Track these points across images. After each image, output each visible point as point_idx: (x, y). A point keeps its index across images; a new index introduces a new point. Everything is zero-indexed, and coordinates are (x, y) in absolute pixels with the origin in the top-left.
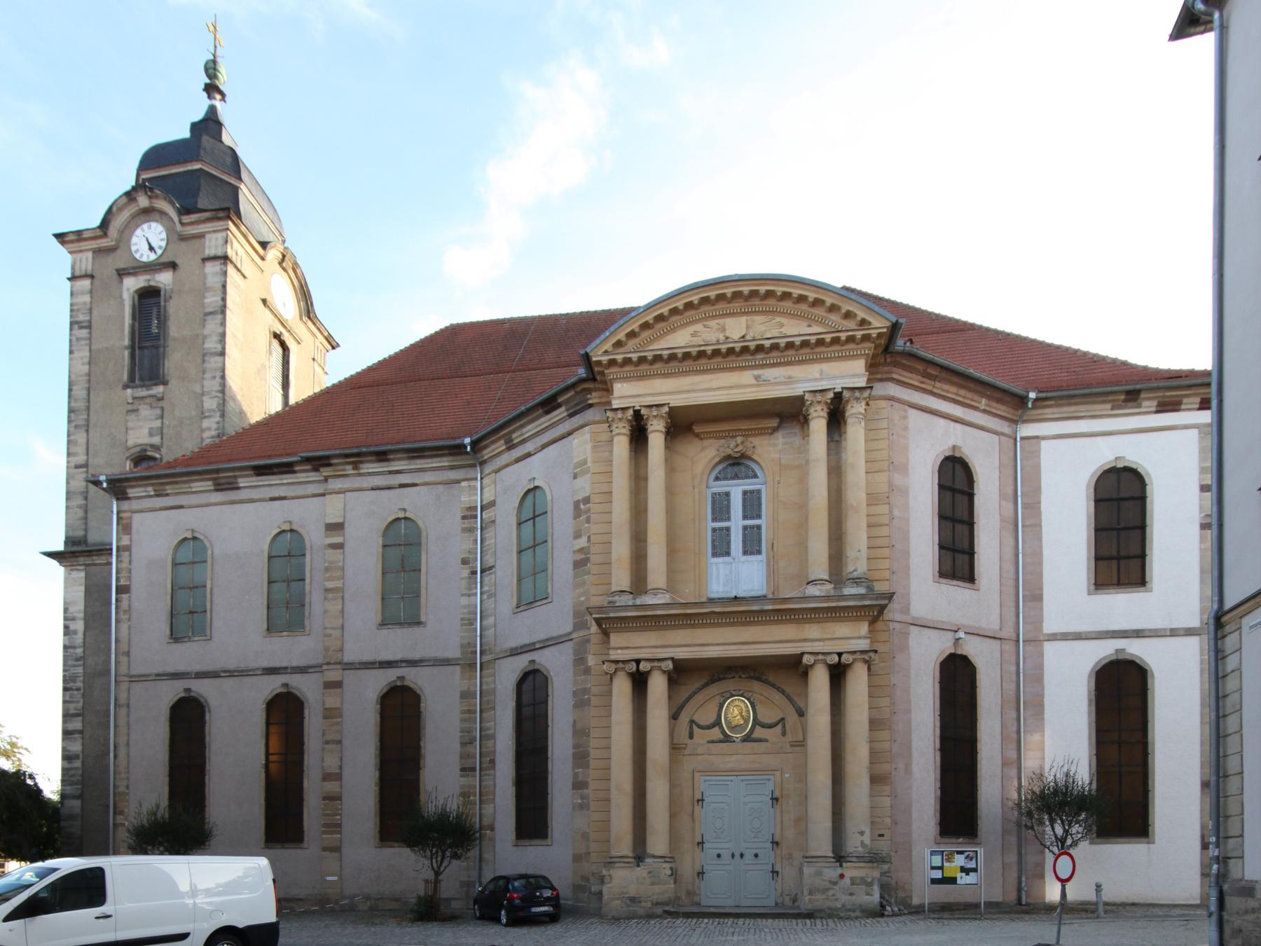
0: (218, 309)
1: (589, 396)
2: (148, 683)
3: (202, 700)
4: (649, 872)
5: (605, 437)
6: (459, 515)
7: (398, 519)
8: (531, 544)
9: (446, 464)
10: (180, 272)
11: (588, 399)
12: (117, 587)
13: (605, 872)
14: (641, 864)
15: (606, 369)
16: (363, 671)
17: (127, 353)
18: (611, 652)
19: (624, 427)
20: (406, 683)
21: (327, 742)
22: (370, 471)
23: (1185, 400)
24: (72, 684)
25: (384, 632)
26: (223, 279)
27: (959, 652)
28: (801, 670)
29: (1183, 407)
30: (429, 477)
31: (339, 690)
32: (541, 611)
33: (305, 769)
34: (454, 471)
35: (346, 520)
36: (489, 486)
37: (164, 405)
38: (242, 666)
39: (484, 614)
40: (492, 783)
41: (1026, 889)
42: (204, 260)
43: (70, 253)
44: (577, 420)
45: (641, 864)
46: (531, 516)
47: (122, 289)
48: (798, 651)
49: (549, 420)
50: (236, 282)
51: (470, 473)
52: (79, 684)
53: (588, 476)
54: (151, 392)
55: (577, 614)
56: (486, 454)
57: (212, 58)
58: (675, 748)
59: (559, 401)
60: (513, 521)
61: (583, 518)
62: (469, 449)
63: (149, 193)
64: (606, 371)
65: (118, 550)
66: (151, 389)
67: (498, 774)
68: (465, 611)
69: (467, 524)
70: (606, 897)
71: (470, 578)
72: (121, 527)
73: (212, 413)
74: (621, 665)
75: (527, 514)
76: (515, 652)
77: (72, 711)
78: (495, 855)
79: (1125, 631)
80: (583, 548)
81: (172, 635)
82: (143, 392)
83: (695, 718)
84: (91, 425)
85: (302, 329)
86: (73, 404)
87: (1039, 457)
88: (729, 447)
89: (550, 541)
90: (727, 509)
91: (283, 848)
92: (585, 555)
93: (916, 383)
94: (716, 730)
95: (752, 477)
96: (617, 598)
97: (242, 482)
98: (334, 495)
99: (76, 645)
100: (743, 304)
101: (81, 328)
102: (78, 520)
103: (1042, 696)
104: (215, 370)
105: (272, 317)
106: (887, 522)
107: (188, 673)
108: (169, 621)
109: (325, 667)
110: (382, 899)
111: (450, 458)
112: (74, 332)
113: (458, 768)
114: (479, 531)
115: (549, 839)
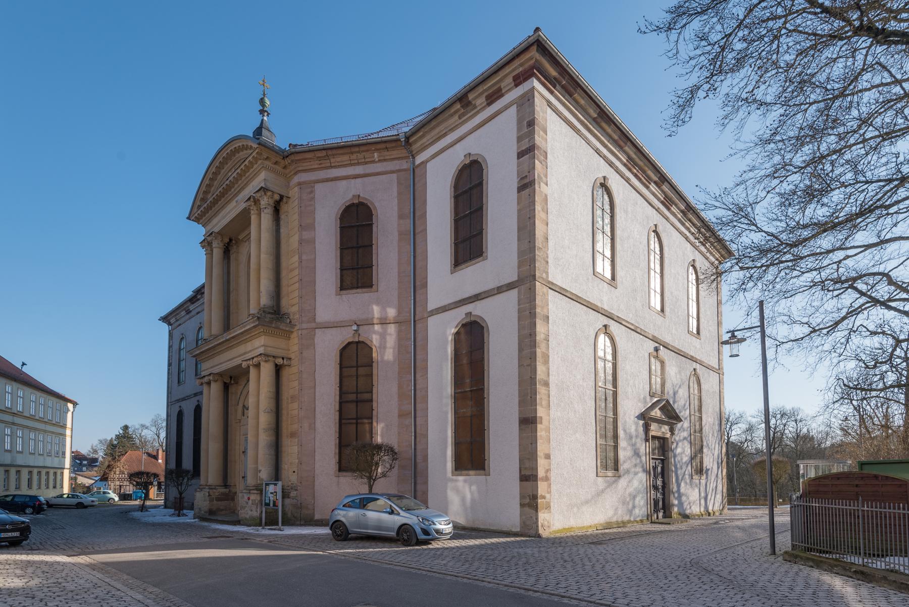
9: (625, 161)
23: (503, 85)
29: (503, 91)
79: (445, 306)
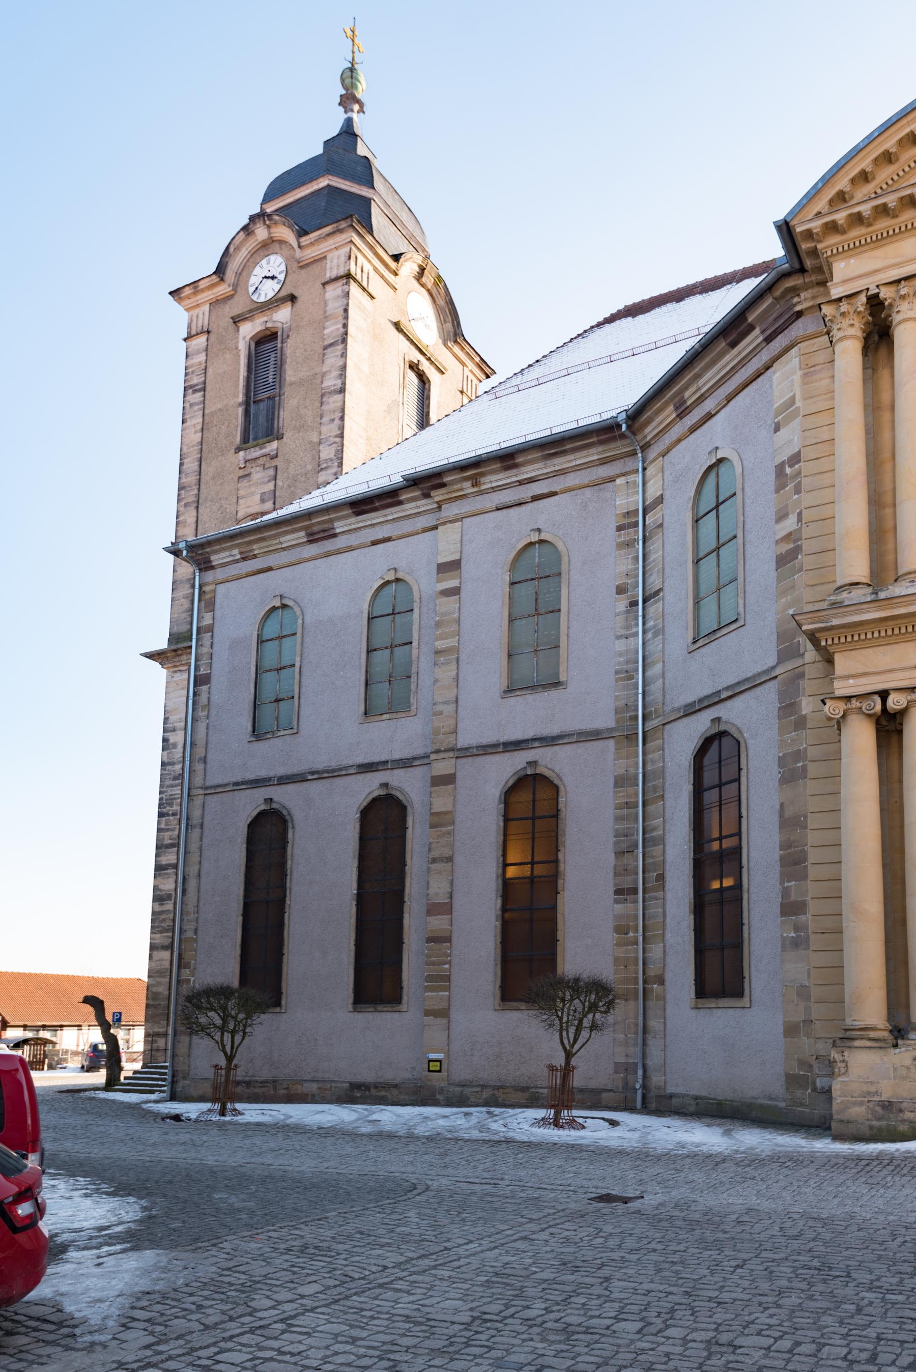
0: (340, 339)
1: (796, 300)
2: (225, 794)
3: (285, 812)
6: (613, 526)
7: (531, 544)
9: (596, 457)
10: (299, 304)
11: (795, 305)
12: (195, 676)
13: (835, 1055)
14: (900, 1042)
15: (820, 241)
16: (483, 758)
17: (240, 411)
18: (836, 684)
19: (852, 325)
20: (540, 770)
21: (434, 861)
22: (494, 485)
24: (168, 808)
25: (512, 701)
26: (345, 302)
30: (572, 480)
31: (450, 787)
32: (729, 642)
33: (406, 899)
34: (605, 467)
35: (464, 556)
36: (654, 476)
37: (278, 464)
38: (334, 764)
39: (648, 661)
40: (661, 910)
42: (324, 284)
43: (187, 310)
45: (900, 1042)
46: (714, 505)
47: (238, 338)
49: (737, 356)
50: (360, 303)
51: (629, 464)
52: (176, 808)
53: (796, 424)
54: (264, 451)
55: (783, 636)
56: (650, 431)
57: (350, 65)
59: (750, 320)
61: (790, 487)
62: (624, 427)
63: (268, 222)
64: (819, 246)
65: (198, 633)
66: (265, 448)
67: (669, 896)
68: (621, 659)
69: (624, 536)
71: (628, 612)
72: (203, 603)
73: (330, 464)
74: (855, 704)
75: (708, 500)
76: (691, 710)
77: (167, 841)
78: (665, 1023)
80: (790, 534)
81: (254, 732)
82: (255, 453)
84: (201, 501)
85: (443, 356)
86: (184, 480)
89: (740, 535)
91: (376, 1011)
92: (795, 542)
96: (845, 595)
97: (339, 527)
98: (449, 525)
99: (175, 760)
101: (195, 391)
102: (184, 612)
104: (334, 411)
105: (408, 343)
107: (270, 779)
108: (252, 715)
109: (433, 757)
110: (501, 1087)
111: (600, 449)
112: (187, 398)
113: (612, 889)
114: (641, 542)
115: (746, 999)
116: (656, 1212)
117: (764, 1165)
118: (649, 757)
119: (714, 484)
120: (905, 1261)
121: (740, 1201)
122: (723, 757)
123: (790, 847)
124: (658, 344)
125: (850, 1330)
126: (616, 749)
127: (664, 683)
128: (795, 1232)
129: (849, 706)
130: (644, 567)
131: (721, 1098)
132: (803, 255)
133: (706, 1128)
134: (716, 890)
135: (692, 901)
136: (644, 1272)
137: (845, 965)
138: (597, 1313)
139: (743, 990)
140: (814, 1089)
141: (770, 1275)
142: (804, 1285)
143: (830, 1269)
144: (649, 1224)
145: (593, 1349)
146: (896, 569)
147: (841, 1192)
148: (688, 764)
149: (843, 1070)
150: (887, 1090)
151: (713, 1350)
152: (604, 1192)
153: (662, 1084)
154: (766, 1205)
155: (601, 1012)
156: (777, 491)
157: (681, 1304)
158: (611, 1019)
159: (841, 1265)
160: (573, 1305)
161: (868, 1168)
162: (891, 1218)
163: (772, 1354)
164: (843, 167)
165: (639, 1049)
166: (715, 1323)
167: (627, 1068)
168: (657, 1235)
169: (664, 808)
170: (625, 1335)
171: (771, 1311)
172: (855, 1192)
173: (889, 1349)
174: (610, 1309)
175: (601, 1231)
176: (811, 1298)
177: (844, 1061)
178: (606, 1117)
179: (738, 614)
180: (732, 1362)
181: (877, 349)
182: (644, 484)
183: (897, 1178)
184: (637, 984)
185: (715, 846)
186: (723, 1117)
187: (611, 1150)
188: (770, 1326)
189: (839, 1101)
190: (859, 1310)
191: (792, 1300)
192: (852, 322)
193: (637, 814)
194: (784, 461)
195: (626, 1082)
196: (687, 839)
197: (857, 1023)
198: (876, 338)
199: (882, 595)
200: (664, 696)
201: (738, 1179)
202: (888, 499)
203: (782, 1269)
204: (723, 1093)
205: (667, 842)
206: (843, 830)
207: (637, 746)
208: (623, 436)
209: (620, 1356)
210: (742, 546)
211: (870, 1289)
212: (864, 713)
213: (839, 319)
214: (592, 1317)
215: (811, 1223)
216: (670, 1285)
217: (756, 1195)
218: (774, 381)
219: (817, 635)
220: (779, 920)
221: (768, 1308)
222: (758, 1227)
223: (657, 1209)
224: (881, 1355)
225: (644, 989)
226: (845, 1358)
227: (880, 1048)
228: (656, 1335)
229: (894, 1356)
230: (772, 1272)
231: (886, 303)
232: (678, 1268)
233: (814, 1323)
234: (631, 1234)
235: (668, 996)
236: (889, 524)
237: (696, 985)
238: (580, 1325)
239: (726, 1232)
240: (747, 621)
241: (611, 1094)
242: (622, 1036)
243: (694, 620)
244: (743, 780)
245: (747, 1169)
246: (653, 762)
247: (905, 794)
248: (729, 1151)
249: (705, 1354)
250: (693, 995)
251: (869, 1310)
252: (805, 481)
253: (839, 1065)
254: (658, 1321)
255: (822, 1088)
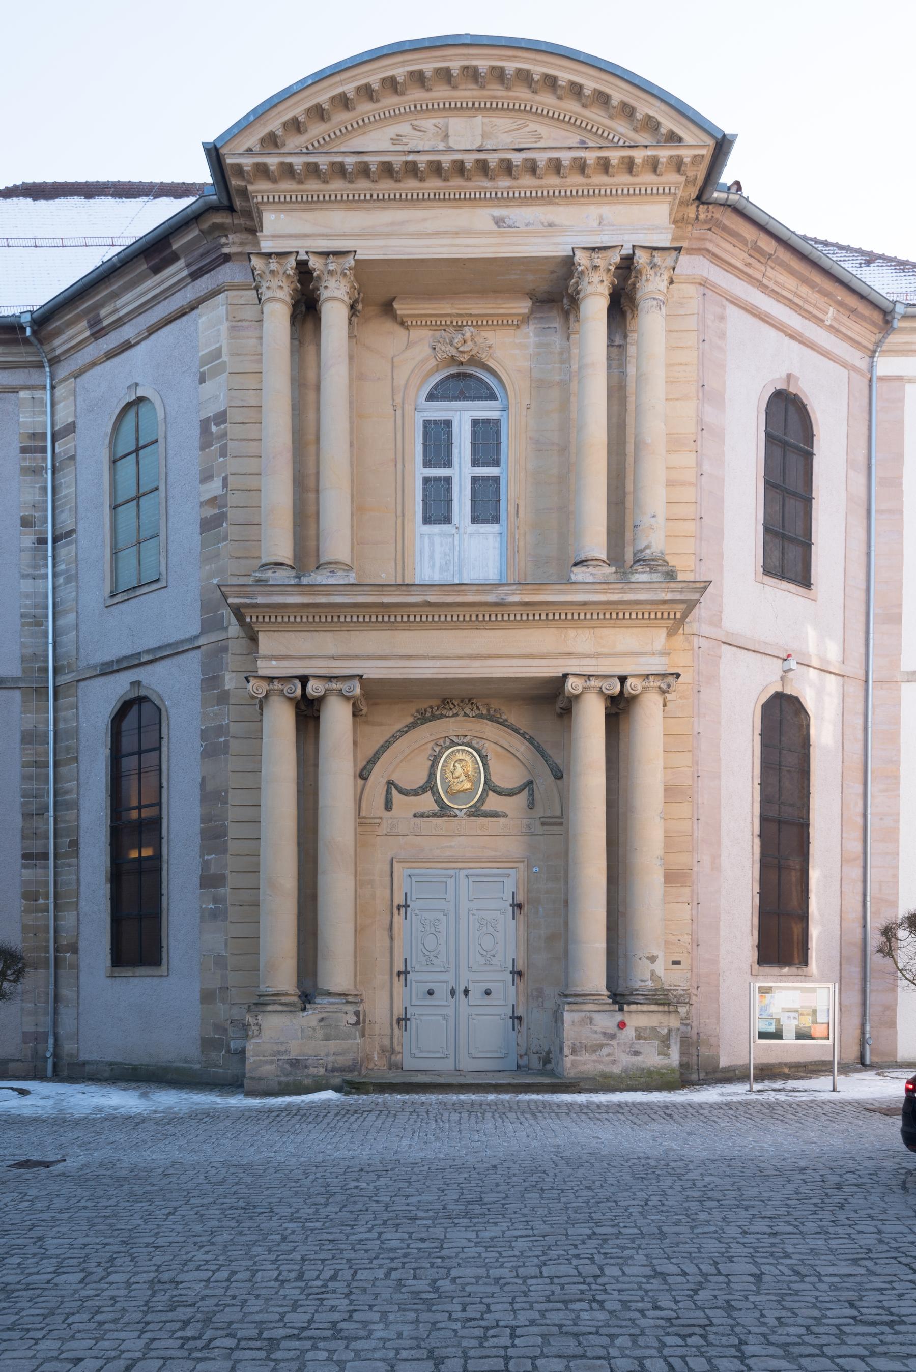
1: (223, 240)
4: (322, 1020)
5: (249, 313)
6: (16, 445)
8: (133, 494)
11: (223, 246)
13: (249, 1019)
14: (308, 1006)
15: (252, 183)
18: (260, 663)
19: (281, 287)
27: (788, 691)
28: (560, 703)
32: (149, 602)
36: (65, 399)
39: (59, 609)
40: (74, 877)
41: (870, 1042)
44: (205, 284)
45: (308, 1006)
46: (134, 448)
48: (558, 672)
51: (35, 377)
55: (206, 606)
56: (60, 344)
58: (363, 823)
59: (174, 247)
60: (105, 456)
62: (28, 332)
67: (83, 863)
68: (28, 602)
69: (30, 461)
70: (251, 1059)
71: (35, 549)
74: (277, 685)
75: (126, 443)
76: (108, 670)
78: (78, 992)
80: (215, 498)
83: (395, 778)
87: (902, 409)
88: (452, 345)
89: (162, 488)
90: (447, 446)
92: (220, 507)
93: (739, 265)
94: (428, 796)
95: (487, 399)
96: (269, 574)
100: (475, 93)
103: (897, 763)
106: (694, 481)
113: (19, 854)
115: (164, 967)
116: (81, 1173)
117: (183, 1123)
118: (61, 714)
119: (134, 424)
120: (318, 1194)
121: (163, 1157)
122: (143, 724)
123: (210, 821)
124: (66, 243)
125: (278, 1256)
126: (23, 702)
127: (78, 636)
128: (219, 1179)
129: (271, 686)
130: (53, 501)
131: (137, 1063)
132: (233, 192)
133: (123, 1092)
134: (134, 860)
135: (109, 869)
136: (78, 1228)
137: (261, 936)
138: (35, 1270)
139: (161, 959)
140: (228, 1051)
141: (202, 1219)
142: (233, 1224)
143: (255, 1207)
144: (76, 1184)
145: (36, 1303)
146: (318, 556)
147: (257, 1141)
148: (105, 727)
149: (256, 1033)
150: (295, 1050)
151: (156, 1288)
152: (23, 1158)
153: (75, 1052)
154: (188, 1158)
155: (9, 981)
156: (202, 448)
157: (119, 1253)
158: (20, 987)
159: (264, 1203)
160: (7, 1266)
161: (278, 1119)
162: (303, 1159)
163: (211, 1285)
164: (275, 106)
165: (50, 1018)
166: (155, 1265)
167: (38, 1037)
168: (85, 1194)
169: (78, 771)
170: (67, 1287)
171: (206, 1249)
172: (268, 1140)
173: (313, 1267)
174: (49, 1265)
175: (26, 1194)
176: (241, 1233)
177: (257, 1024)
178: (15, 1086)
179: (160, 574)
180: (176, 1296)
181: (304, 321)
182: (53, 405)
183: (304, 1126)
184: (48, 952)
185: (134, 814)
186: (138, 1081)
187: (25, 1118)
188: (207, 1261)
189: (252, 1060)
190: (284, 1239)
191: (223, 1237)
192: (281, 284)
193: (48, 775)
194: (209, 417)
195: (35, 1051)
196: (104, 805)
197: (270, 989)
198: (304, 309)
199: (305, 581)
200: (78, 650)
201: (159, 1136)
202: (311, 483)
203: (211, 1212)
204: (139, 1056)
205: (81, 807)
206: (262, 808)
207: (48, 701)
208: (26, 342)
209: (66, 1305)
210: (164, 500)
211: (292, 1220)
212: (285, 696)
213: (268, 276)
214: (30, 1274)
215: (232, 1170)
216: (106, 1237)
217: (178, 1150)
218: (200, 325)
219: (243, 610)
220: (198, 891)
221: (203, 1246)
222: (184, 1178)
223: (82, 1170)
224: (307, 1273)
225: (56, 958)
226: (276, 1280)
227: (291, 1011)
228: (99, 1282)
229: (318, 1272)
230: (202, 1215)
231: (315, 274)
232: (111, 1221)
233: (246, 1254)
234: (58, 1196)
235: (82, 965)
236: (312, 509)
237: (112, 953)
238: (19, 1283)
239: (154, 1185)
240: (170, 583)
241: (19, 1063)
242: (31, 1005)
243: (112, 571)
244: (164, 749)
245: (167, 1127)
246: (66, 720)
247: (320, 778)
248: (147, 1112)
249: (149, 1292)
250: (109, 963)
251: (293, 1237)
252: (231, 445)
253: (253, 1028)
254: (99, 1269)
255: (236, 1050)
